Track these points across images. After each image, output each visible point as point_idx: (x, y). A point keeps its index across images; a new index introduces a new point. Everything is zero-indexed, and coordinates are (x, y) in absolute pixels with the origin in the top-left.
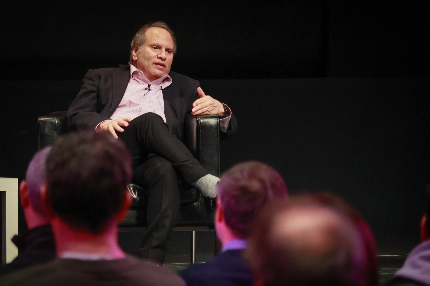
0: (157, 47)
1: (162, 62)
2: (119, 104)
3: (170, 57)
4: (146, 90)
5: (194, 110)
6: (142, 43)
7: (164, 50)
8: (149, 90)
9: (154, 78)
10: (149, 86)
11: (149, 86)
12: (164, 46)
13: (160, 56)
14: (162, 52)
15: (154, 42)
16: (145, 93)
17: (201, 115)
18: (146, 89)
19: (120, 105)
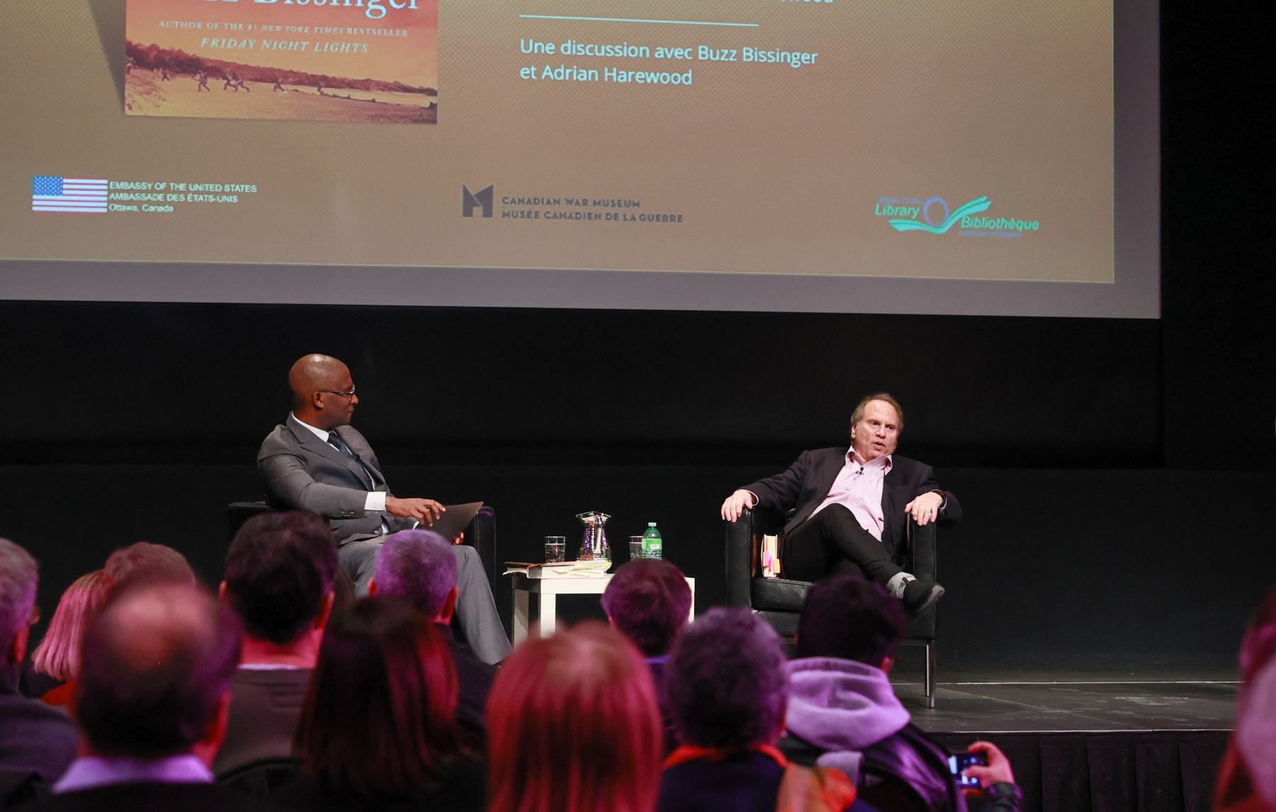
0: (877, 423)
1: (880, 440)
2: (828, 492)
3: (893, 434)
4: (278, 90)
5: (920, 524)
6: (861, 418)
7: (883, 426)
8: (861, 473)
9: (870, 458)
10: (862, 469)
11: (862, 469)
12: (884, 422)
13: (878, 433)
14: (880, 428)
15: (872, 417)
16: (352, 97)
17: (387, 120)
18: (857, 473)
19: (829, 495)
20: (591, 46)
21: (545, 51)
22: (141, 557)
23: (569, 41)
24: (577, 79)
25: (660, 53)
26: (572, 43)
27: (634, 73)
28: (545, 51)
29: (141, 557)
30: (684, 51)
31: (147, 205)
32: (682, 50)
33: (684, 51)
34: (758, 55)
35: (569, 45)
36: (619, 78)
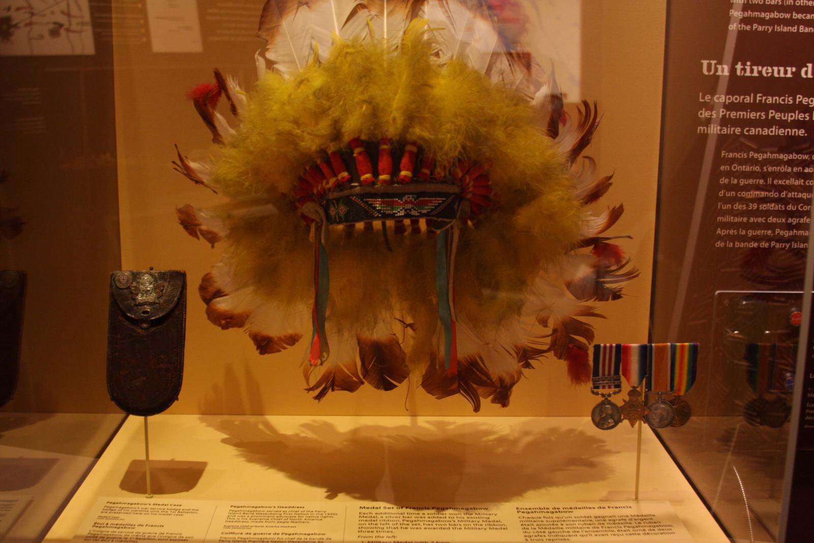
20: (783, 98)
21: (798, 134)
22: (501, 64)
23: (774, 127)
24: (762, 134)
25: (738, 130)
26: (776, 128)
27: (734, 128)
28: (798, 134)
29: (501, 64)
30: (809, 99)
31: (748, 129)
32: (710, 112)
33: (809, 99)
34: (788, 99)
35: (774, 130)
36: (763, 132)
